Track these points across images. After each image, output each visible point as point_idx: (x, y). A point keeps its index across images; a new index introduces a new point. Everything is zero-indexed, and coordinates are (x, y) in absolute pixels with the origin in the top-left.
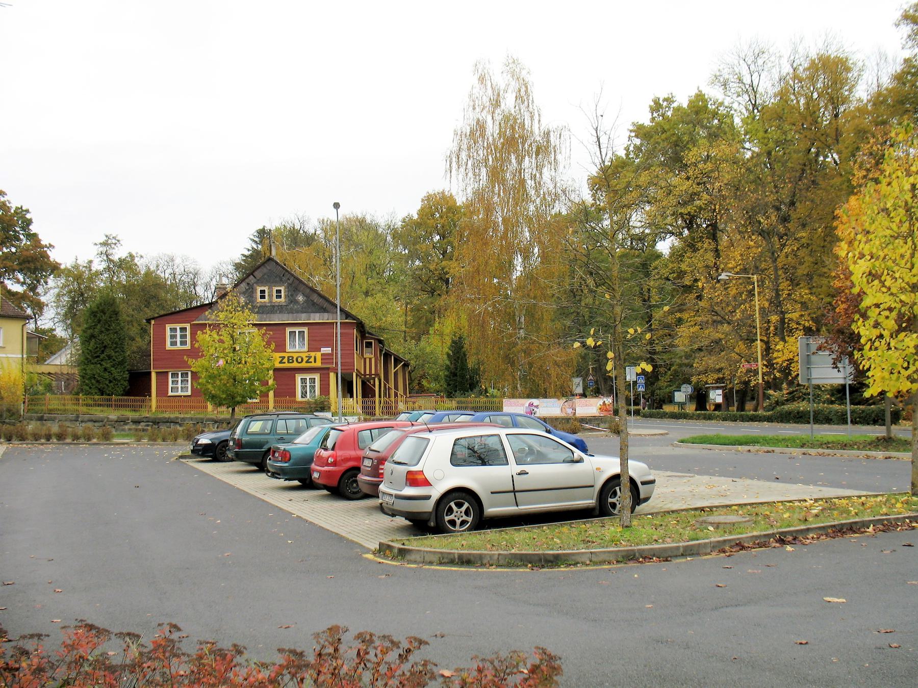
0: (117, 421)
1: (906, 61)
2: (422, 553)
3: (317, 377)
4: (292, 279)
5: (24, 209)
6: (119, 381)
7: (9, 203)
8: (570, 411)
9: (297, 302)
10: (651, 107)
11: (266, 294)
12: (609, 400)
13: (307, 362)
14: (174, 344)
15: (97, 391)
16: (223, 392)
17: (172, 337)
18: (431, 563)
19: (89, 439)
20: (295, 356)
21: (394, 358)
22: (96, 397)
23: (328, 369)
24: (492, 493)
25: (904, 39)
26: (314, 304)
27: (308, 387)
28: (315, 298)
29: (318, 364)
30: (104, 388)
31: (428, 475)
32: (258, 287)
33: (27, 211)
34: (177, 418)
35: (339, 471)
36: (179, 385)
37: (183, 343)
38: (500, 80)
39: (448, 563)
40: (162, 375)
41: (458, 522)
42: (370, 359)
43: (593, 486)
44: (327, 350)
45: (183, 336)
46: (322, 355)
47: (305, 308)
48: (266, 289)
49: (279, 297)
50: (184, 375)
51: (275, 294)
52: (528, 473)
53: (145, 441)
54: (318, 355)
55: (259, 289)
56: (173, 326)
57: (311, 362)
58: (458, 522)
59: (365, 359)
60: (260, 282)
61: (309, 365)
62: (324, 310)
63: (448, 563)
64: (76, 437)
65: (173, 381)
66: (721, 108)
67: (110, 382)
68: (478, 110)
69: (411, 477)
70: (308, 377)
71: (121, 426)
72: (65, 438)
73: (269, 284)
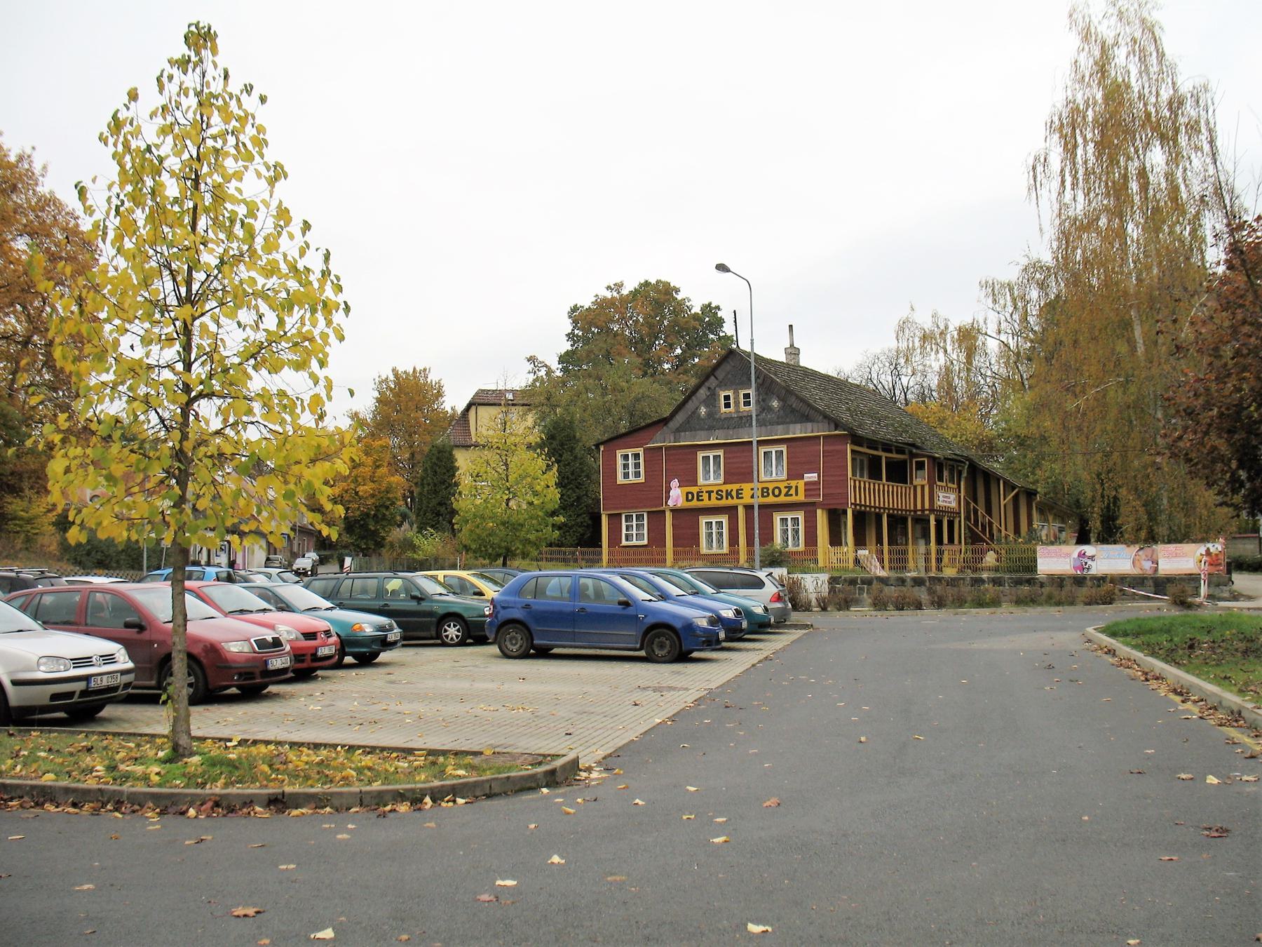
3: (800, 516)
5: (713, 305)
7: (689, 300)
8: (1148, 566)
9: (770, 409)
11: (732, 401)
12: (1216, 545)
13: (786, 495)
14: (626, 475)
17: (626, 466)
20: (771, 486)
21: (1004, 483)
26: (793, 411)
27: (789, 530)
28: (793, 401)
29: (801, 497)
32: (721, 392)
33: (718, 308)
37: (637, 475)
38: (1107, 29)
40: (615, 518)
42: (923, 487)
45: (637, 465)
46: (806, 484)
48: (730, 393)
49: (747, 404)
51: (742, 400)
54: (801, 484)
55: (723, 394)
56: (624, 452)
57: (791, 495)
59: (915, 487)
60: (724, 385)
61: (788, 499)
70: (789, 516)
73: (734, 387)
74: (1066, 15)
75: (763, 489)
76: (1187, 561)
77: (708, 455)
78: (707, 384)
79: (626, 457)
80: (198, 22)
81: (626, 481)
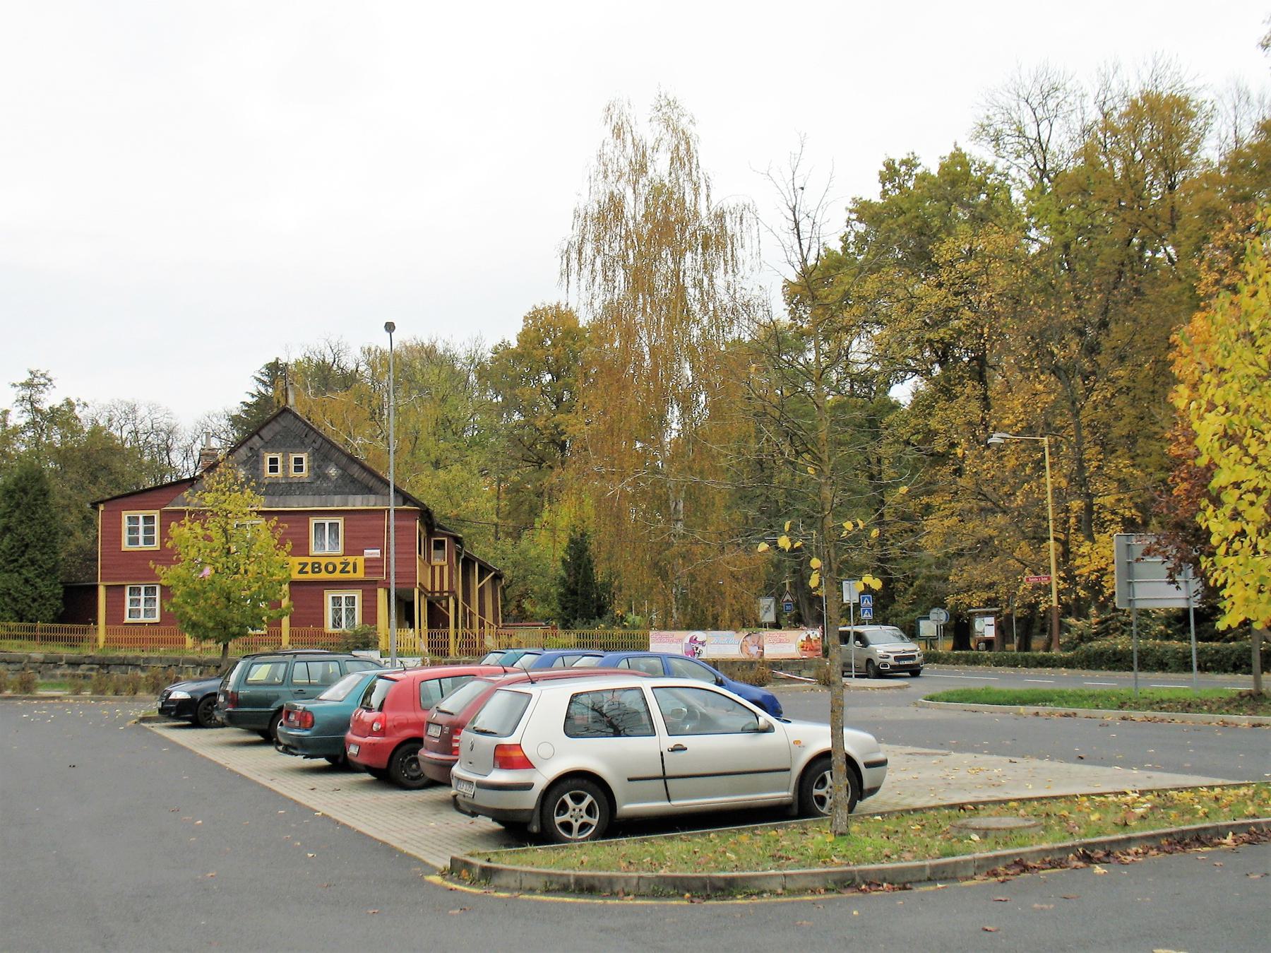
0: (43, 663)
2: (518, 874)
3: (358, 595)
8: (754, 650)
9: (326, 477)
11: (279, 465)
12: (816, 632)
13: (342, 571)
14: (134, 541)
16: (210, 618)
20: (324, 561)
22: (12, 624)
24: (630, 780)
26: (354, 480)
28: (355, 471)
29: (360, 575)
30: (23, 610)
31: (529, 751)
34: (138, 658)
35: (390, 744)
37: (149, 541)
38: (647, 131)
40: (115, 592)
41: (576, 825)
42: (442, 568)
43: (788, 770)
46: (366, 560)
48: (279, 456)
51: (292, 465)
52: (686, 749)
53: (88, 693)
54: (360, 561)
55: (268, 457)
56: (133, 513)
57: (348, 572)
58: (576, 825)
59: (433, 568)
60: (270, 445)
63: (558, 890)
68: (611, 178)
69: (499, 753)
70: (343, 594)
71: (50, 669)
73: (283, 449)
74: (605, 106)
75: (313, 564)
76: (790, 647)
77: (323, 521)
78: (249, 443)
79: (134, 520)
80: (847, 209)
81: (134, 548)
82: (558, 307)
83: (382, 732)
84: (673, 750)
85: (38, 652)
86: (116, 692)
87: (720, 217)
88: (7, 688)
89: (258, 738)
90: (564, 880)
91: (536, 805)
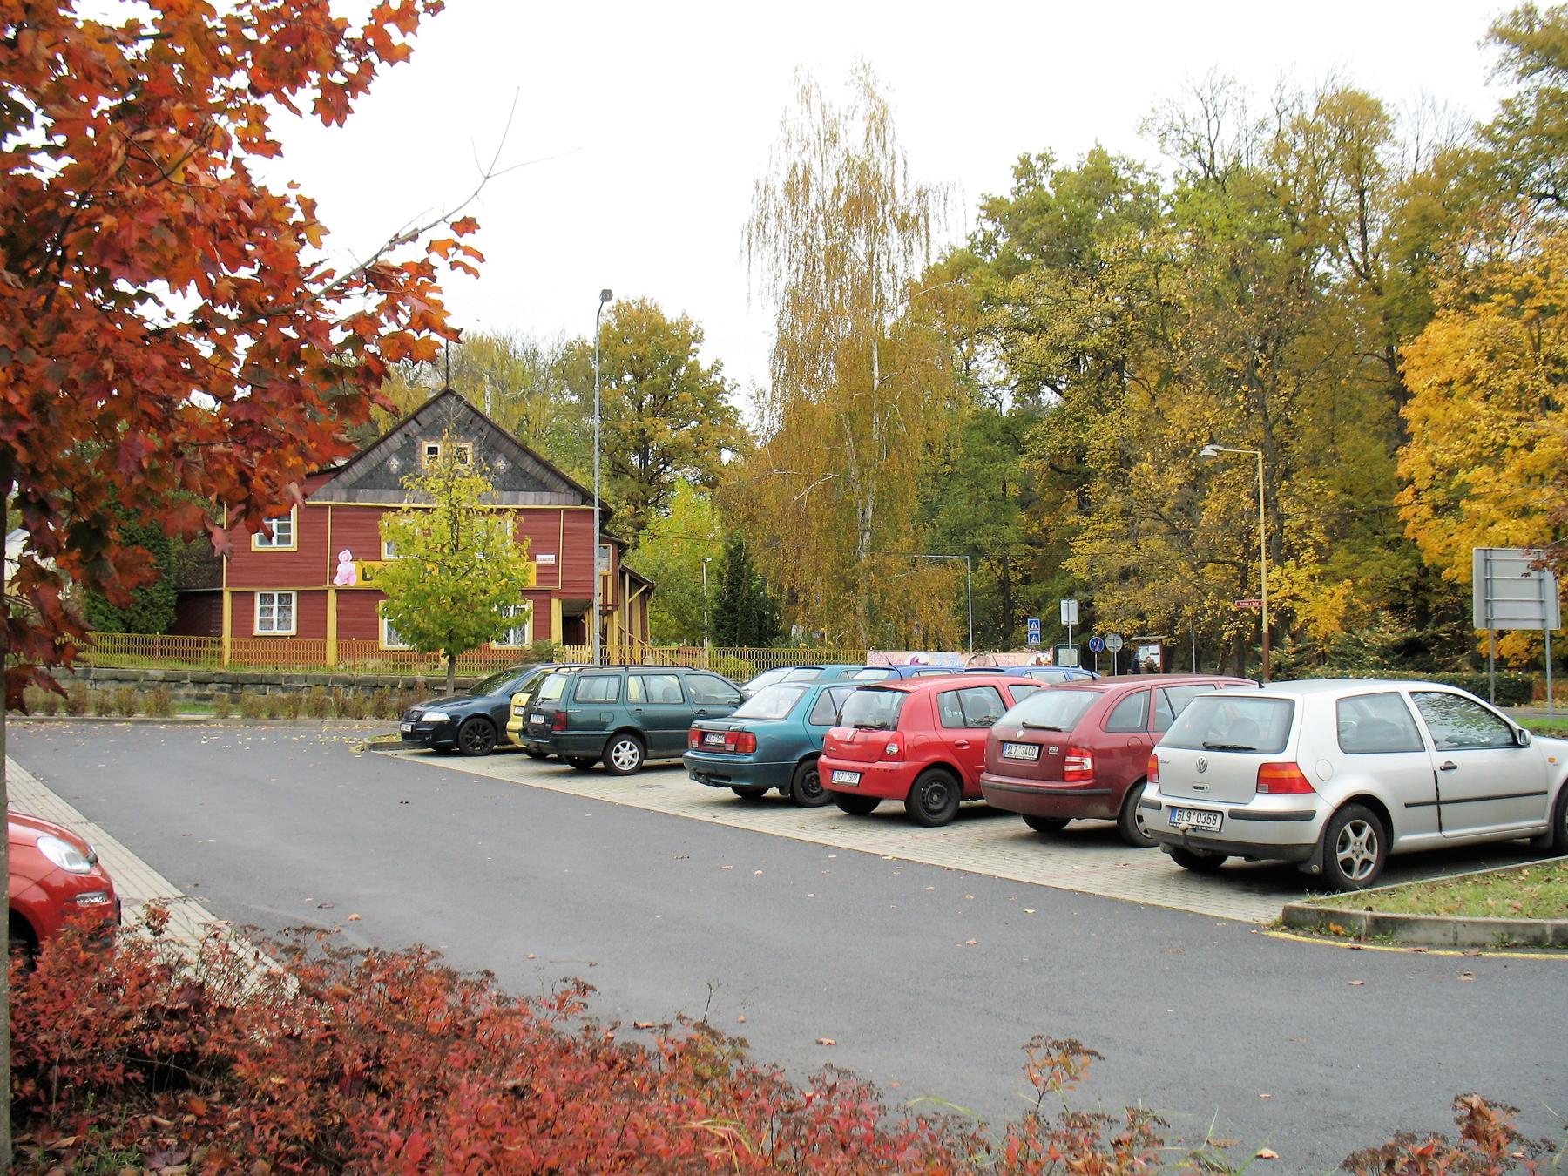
0: (163, 681)
1: (1506, 104)
2: (1450, 926)
4: (487, 428)
6: (161, 607)
10: (1016, 169)
15: (120, 625)
16: (440, 625)
18: (1483, 946)
19: (130, 713)
22: (119, 635)
23: (549, 592)
24: (1407, 805)
25: (1490, 68)
26: (525, 475)
28: (528, 465)
30: (132, 619)
31: (1308, 771)
32: (424, 442)
34: (278, 676)
35: (910, 769)
36: (275, 616)
38: (842, 97)
39: (1525, 945)
40: (243, 599)
41: (1357, 862)
43: (1545, 793)
44: (548, 559)
46: (538, 567)
47: (509, 482)
50: (285, 598)
52: (1455, 767)
53: (237, 716)
58: (1357, 862)
62: (541, 486)
63: (1525, 945)
64: (104, 709)
65: (262, 610)
66: (1141, 176)
67: (144, 608)
68: (796, 147)
69: (1265, 774)
71: (171, 689)
72: (84, 711)
82: (642, 302)
83: (899, 757)
84: (1446, 769)
85: (156, 669)
86: (272, 716)
87: (921, 195)
88: (139, 711)
89: (568, 767)
90: (1537, 932)
91: (1320, 838)
